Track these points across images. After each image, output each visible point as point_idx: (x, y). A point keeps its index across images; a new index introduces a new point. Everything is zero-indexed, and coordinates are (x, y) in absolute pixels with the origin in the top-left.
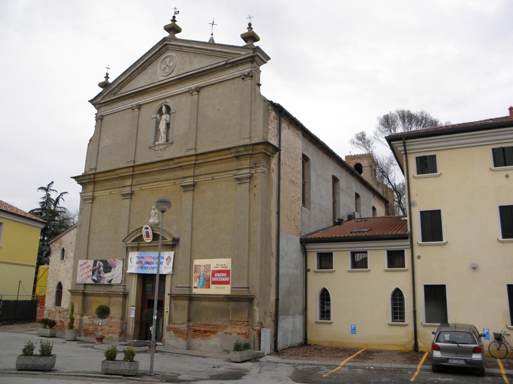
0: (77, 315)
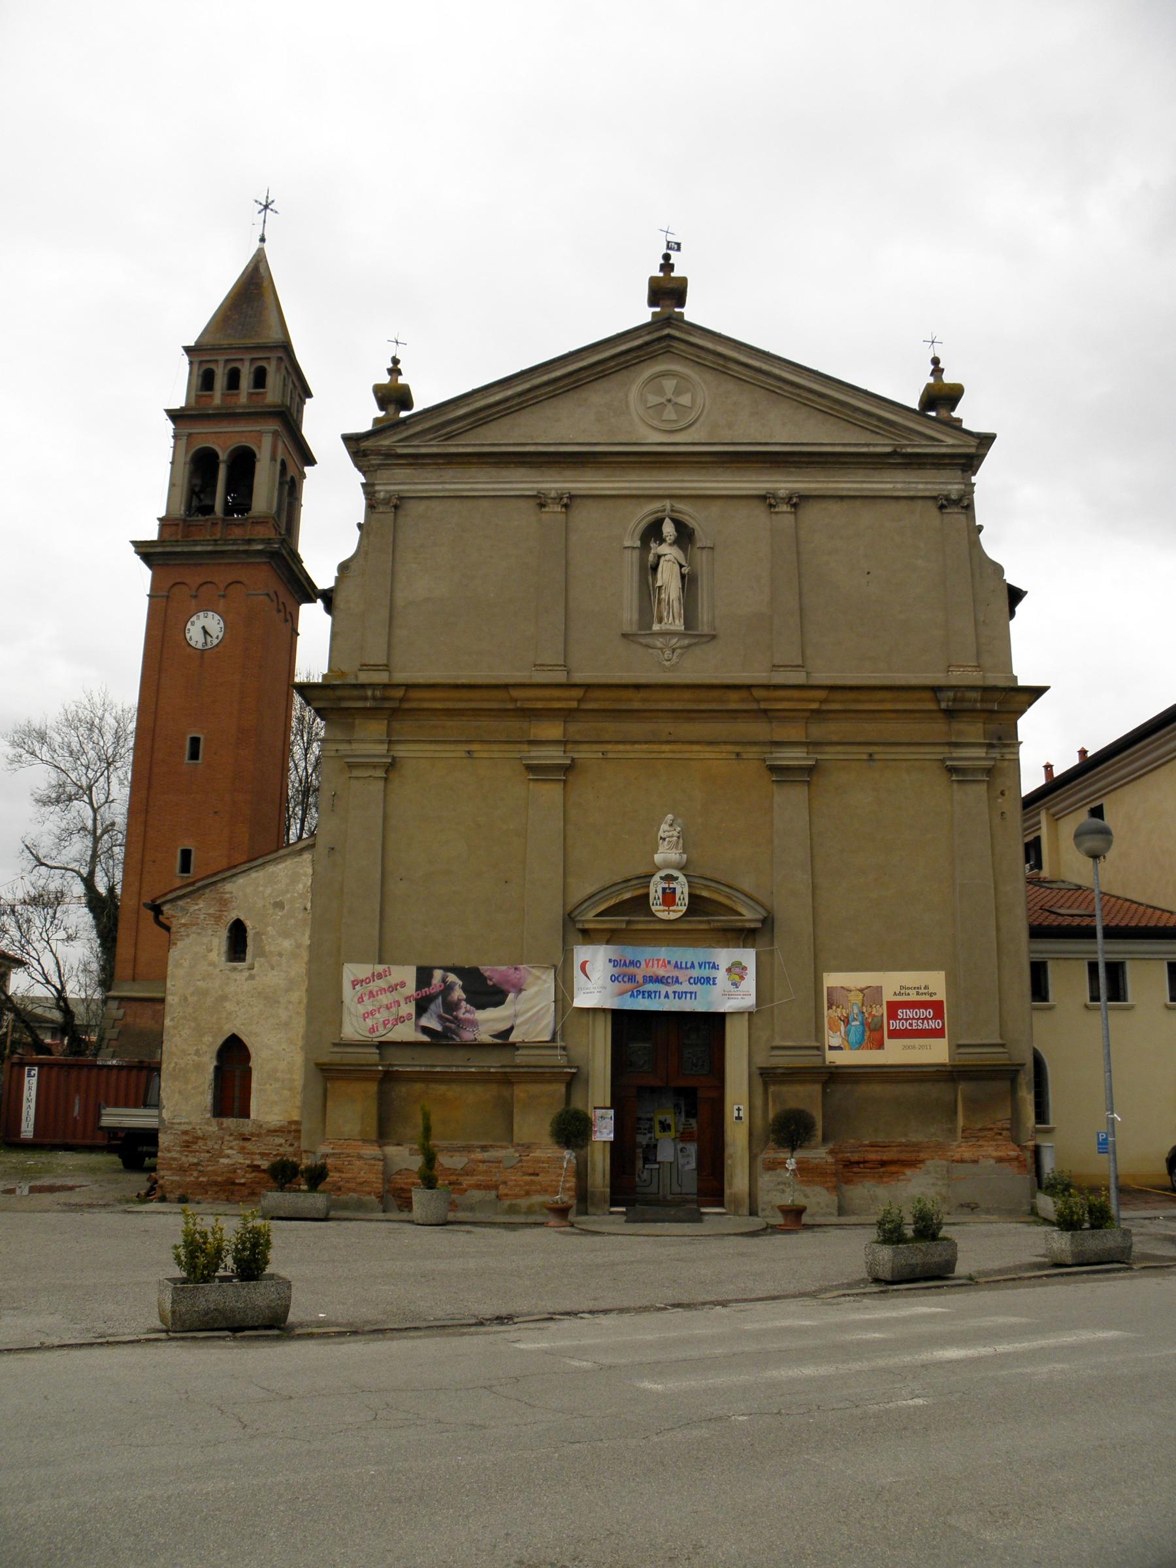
0: (360, 1143)
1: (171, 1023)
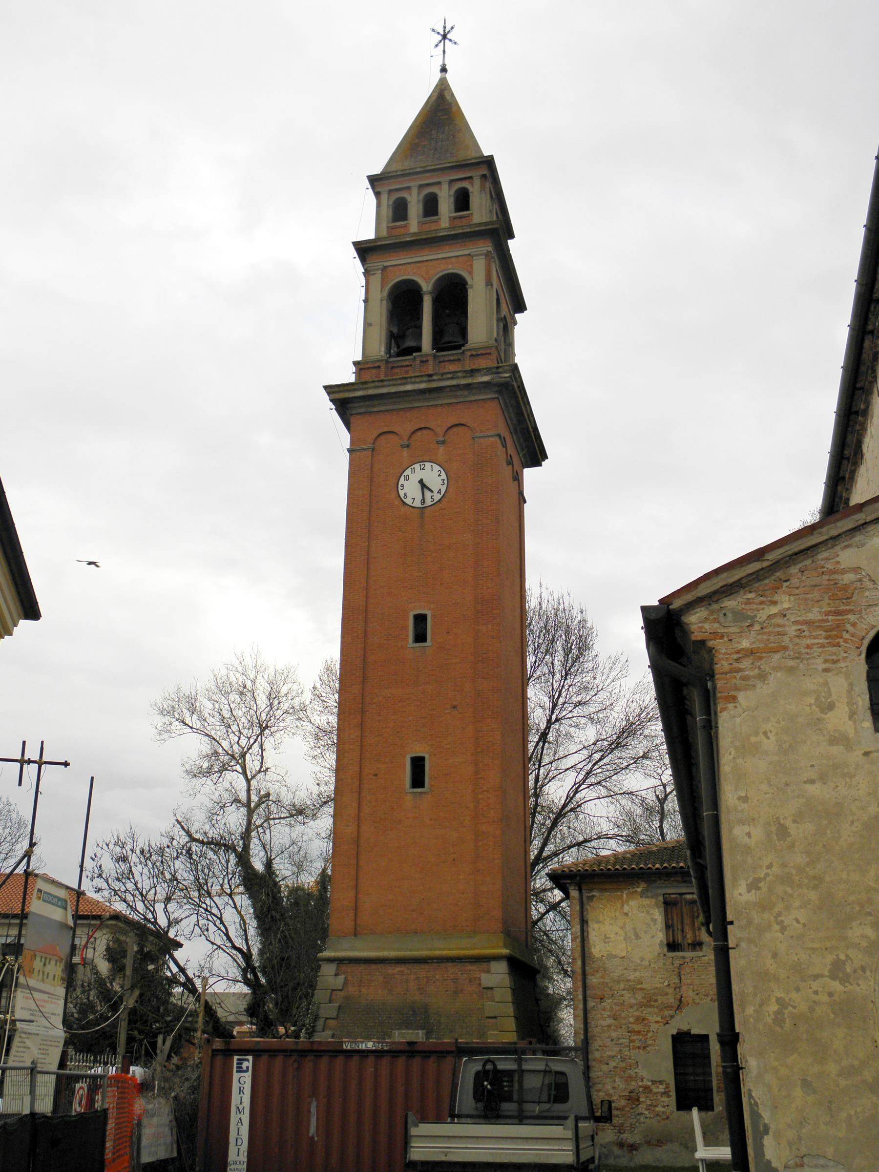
1: (751, 897)
